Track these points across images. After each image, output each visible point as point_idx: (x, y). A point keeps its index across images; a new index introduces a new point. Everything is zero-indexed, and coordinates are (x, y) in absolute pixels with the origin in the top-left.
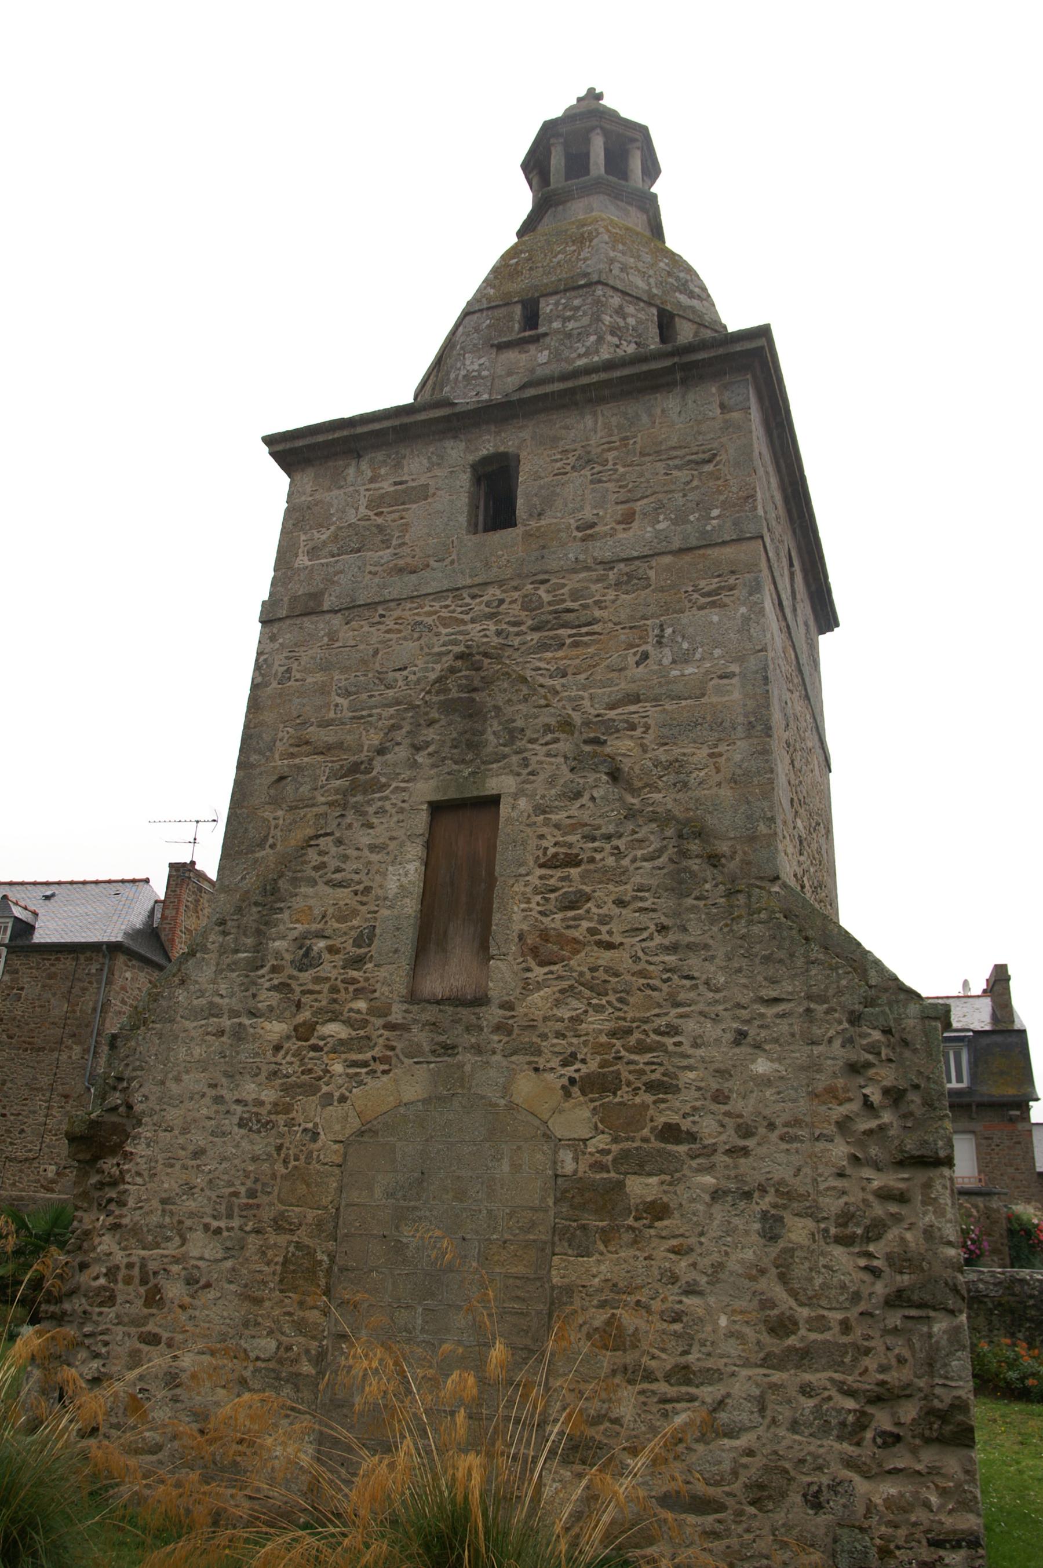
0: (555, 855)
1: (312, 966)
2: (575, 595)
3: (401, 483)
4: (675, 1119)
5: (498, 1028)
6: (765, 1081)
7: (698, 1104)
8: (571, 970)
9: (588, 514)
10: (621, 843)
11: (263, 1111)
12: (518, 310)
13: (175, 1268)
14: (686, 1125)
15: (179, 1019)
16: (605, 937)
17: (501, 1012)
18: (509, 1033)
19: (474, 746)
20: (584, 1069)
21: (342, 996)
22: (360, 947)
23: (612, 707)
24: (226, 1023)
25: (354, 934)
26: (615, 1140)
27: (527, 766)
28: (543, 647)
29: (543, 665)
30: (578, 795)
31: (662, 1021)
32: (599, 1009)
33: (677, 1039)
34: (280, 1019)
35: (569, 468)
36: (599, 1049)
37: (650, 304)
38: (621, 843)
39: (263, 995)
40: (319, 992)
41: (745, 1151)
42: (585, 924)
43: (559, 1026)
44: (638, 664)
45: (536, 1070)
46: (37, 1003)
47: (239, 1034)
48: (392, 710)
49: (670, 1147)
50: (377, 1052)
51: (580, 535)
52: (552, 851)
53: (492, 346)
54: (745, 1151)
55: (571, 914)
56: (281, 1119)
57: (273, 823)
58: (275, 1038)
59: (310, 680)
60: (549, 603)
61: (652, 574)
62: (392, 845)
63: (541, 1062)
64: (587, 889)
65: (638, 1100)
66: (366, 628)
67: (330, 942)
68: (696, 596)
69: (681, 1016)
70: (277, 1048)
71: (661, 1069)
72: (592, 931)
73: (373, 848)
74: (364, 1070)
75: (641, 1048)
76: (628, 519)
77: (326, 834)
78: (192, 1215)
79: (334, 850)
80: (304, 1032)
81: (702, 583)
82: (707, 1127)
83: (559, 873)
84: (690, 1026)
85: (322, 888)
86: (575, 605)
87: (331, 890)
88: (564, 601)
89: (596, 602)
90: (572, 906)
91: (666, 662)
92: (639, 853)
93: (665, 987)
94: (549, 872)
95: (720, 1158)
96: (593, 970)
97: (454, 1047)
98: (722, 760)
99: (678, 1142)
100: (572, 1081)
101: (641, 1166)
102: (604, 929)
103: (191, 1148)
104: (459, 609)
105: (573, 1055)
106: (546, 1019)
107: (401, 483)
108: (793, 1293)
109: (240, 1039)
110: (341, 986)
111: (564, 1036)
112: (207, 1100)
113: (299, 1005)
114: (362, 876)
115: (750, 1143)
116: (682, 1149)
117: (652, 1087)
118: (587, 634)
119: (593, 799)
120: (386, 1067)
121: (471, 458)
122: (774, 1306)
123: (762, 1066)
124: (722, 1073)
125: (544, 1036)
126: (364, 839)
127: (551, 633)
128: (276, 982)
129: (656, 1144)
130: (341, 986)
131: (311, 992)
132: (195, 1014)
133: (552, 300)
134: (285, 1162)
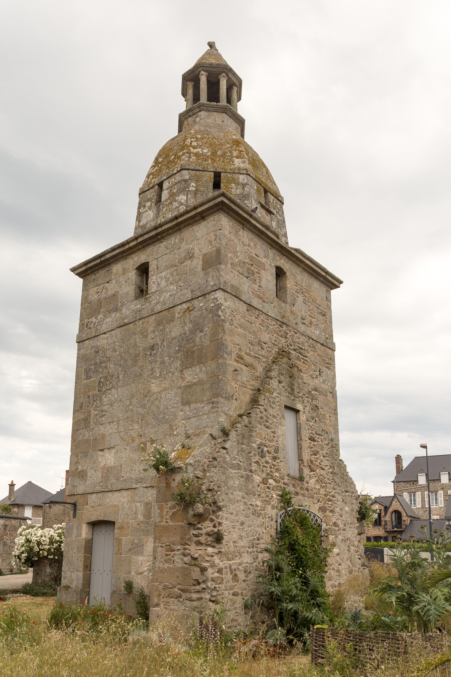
3: (257, 256)
104: (278, 329)
105: (319, 500)
130: (273, 466)
132: (233, 467)
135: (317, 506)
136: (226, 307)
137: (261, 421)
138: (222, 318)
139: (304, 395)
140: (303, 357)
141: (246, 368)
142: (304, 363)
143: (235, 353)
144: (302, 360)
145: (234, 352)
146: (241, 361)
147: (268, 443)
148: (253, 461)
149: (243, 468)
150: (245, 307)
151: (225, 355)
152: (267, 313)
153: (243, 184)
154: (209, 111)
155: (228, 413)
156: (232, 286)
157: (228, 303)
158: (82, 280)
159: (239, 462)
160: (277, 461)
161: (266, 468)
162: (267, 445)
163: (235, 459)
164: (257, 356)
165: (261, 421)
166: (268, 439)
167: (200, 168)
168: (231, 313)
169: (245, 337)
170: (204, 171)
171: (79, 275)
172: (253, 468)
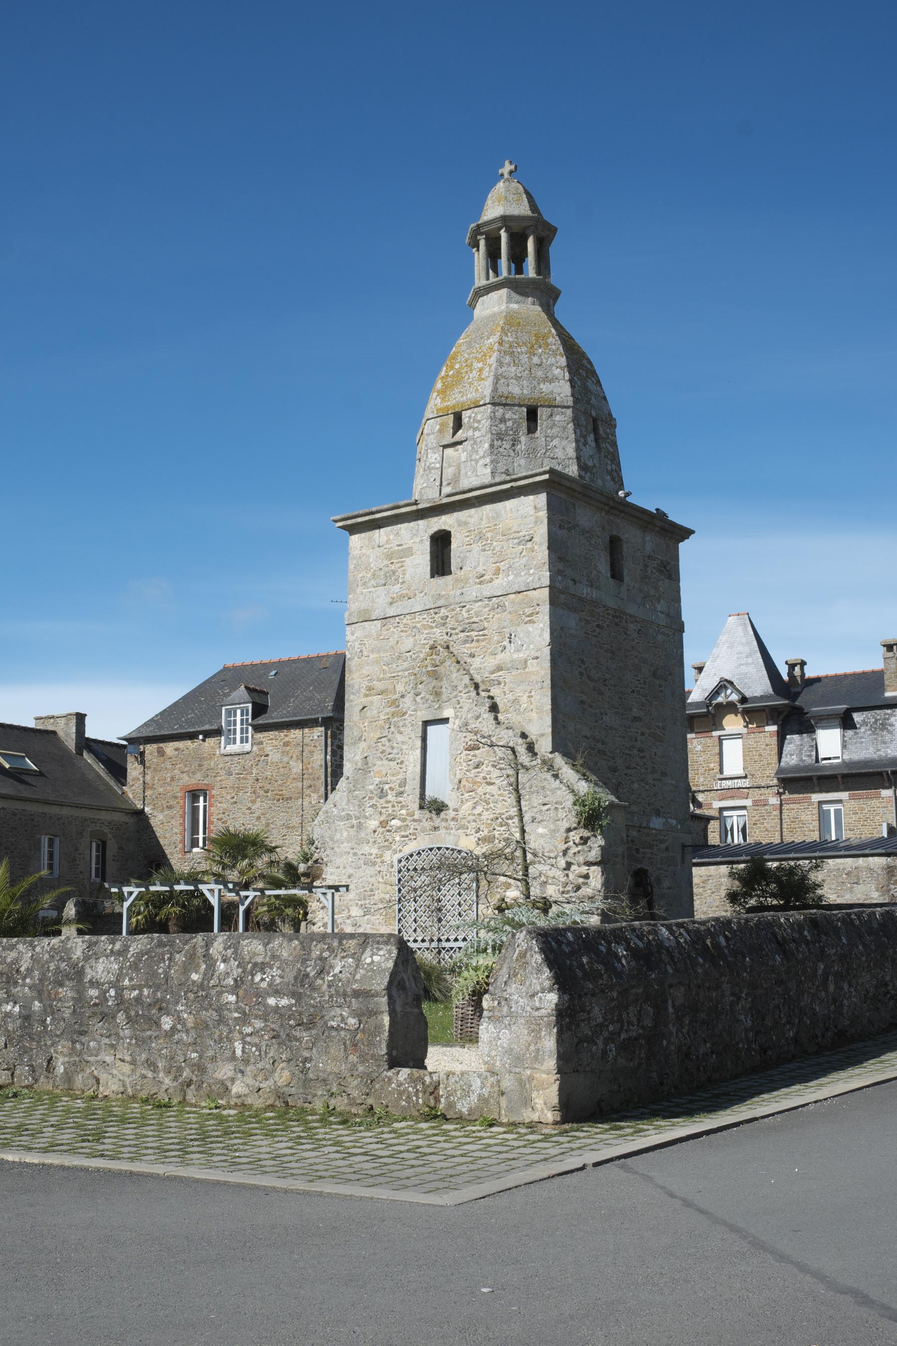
3: (400, 545)
5: (453, 819)
6: (542, 836)
9: (480, 569)
11: (372, 857)
12: (451, 417)
13: (348, 921)
19: (437, 694)
21: (396, 809)
23: (493, 673)
24: (354, 822)
28: (465, 642)
32: (487, 810)
37: (520, 406)
39: (367, 809)
42: (482, 775)
43: (473, 818)
44: (502, 651)
46: (280, 765)
48: (406, 673)
50: (411, 831)
52: (469, 743)
56: (379, 860)
58: (373, 827)
59: (371, 656)
60: (467, 618)
63: (468, 832)
66: (392, 629)
68: (524, 617)
70: (375, 832)
72: (485, 778)
73: (403, 743)
76: (497, 572)
78: (351, 900)
80: (384, 824)
83: (472, 753)
85: (385, 762)
86: (476, 620)
90: (477, 767)
96: (485, 794)
100: (479, 839)
107: (400, 545)
112: (351, 855)
113: (381, 813)
114: (399, 755)
121: (431, 531)
123: (541, 830)
125: (469, 822)
132: (341, 819)
134: (383, 878)
135: (473, 839)
139: (460, 692)
140: (477, 633)
142: (478, 641)
147: (390, 778)
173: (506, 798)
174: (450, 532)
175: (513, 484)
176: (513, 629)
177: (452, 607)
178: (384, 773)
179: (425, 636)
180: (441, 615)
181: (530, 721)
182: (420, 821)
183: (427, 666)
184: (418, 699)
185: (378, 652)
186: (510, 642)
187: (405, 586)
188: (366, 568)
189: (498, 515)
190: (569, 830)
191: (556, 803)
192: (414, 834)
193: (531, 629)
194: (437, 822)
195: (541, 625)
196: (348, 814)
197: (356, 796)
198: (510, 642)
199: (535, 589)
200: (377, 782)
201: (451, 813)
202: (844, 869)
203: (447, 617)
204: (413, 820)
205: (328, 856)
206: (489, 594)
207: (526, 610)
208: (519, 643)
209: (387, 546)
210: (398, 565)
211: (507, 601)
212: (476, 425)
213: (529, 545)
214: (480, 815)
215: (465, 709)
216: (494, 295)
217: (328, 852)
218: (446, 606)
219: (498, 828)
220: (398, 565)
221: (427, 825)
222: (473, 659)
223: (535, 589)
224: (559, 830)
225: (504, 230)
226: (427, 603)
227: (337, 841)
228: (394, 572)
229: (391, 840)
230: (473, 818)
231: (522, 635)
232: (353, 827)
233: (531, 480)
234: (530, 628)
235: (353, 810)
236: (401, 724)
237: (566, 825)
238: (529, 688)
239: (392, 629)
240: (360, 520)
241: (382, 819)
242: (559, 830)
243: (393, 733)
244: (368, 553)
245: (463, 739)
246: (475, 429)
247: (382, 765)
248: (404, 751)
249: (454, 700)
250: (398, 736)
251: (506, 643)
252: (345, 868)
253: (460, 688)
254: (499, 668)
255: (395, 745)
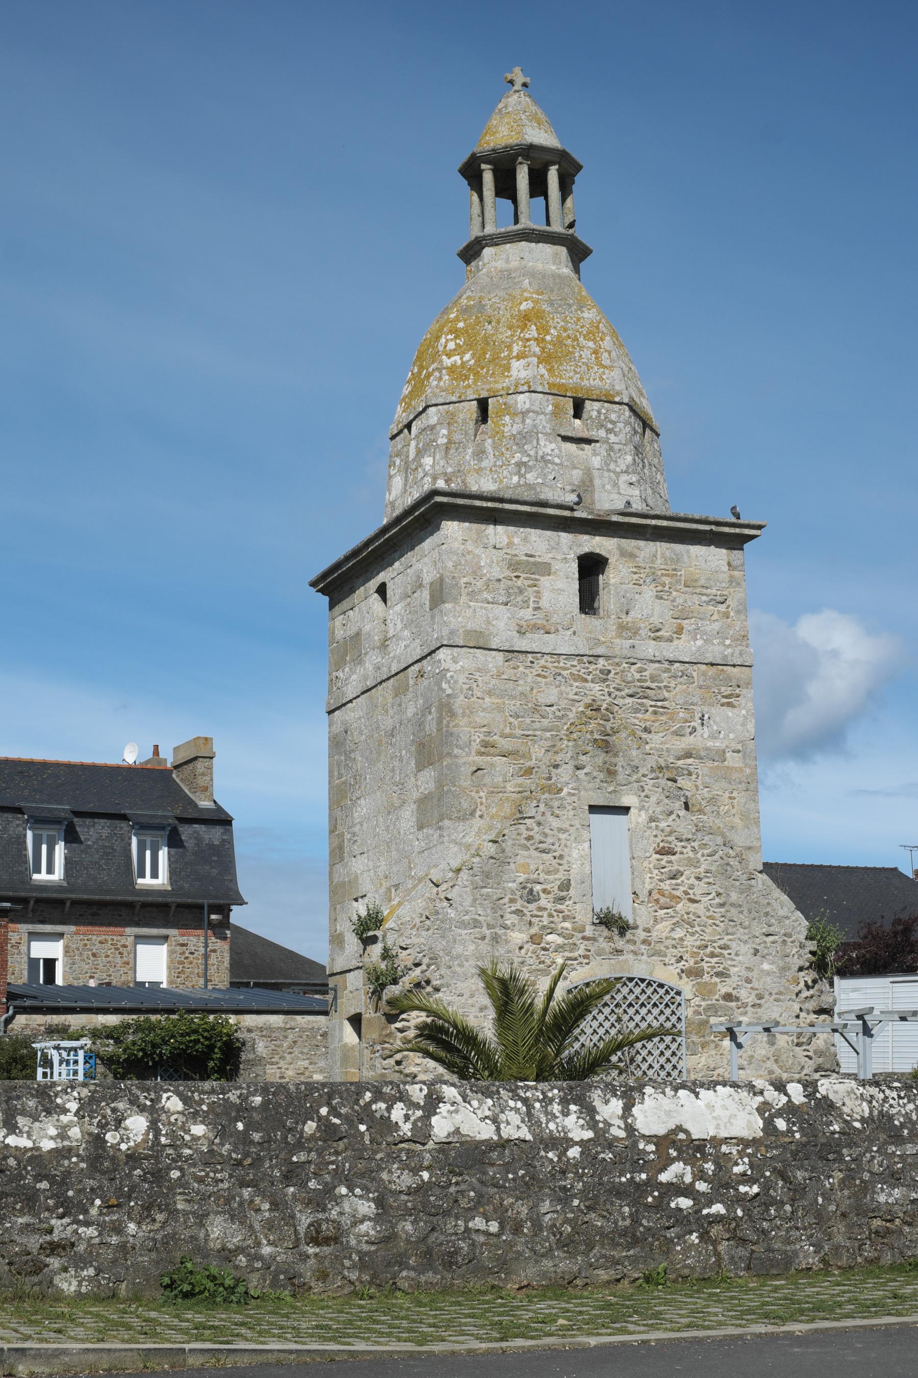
0: (663, 848)
1: (536, 901)
2: (653, 679)
3: (531, 556)
4: (730, 990)
5: (644, 942)
6: (768, 973)
7: (739, 983)
8: (677, 913)
10: (695, 844)
14: (734, 993)
15: (453, 928)
16: (692, 896)
17: (644, 933)
18: (650, 945)
19: (611, 773)
20: (687, 965)
22: (562, 891)
23: (679, 759)
25: (558, 883)
26: (704, 1000)
27: (643, 791)
28: (637, 711)
29: (637, 722)
30: (671, 813)
31: (721, 942)
32: (692, 934)
33: (729, 951)
34: (520, 931)
35: (642, 581)
36: (694, 955)
38: (695, 844)
39: (507, 916)
40: (542, 917)
41: (760, 1005)
42: (682, 889)
43: (674, 942)
44: (691, 734)
45: (665, 964)
47: (496, 939)
48: (548, 734)
49: (728, 1004)
51: (652, 635)
52: (661, 845)
53: (559, 435)
54: (760, 1005)
55: (674, 882)
57: (479, 800)
58: (519, 942)
59: (487, 699)
60: (639, 680)
61: (695, 674)
62: (572, 830)
63: (667, 960)
64: (681, 869)
65: (713, 981)
67: (543, 886)
69: (730, 940)
70: (521, 948)
71: (722, 966)
73: (560, 830)
74: (575, 962)
75: (712, 955)
77: (530, 818)
79: (536, 828)
80: (535, 939)
81: (723, 689)
82: (743, 994)
83: (665, 858)
84: (733, 945)
86: (653, 685)
87: (539, 854)
88: (646, 681)
89: (665, 687)
91: (706, 736)
92: (706, 852)
93: (722, 925)
94: (661, 857)
95: (749, 1009)
96: (688, 913)
97: (622, 951)
98: (735, 801)
99: (732, 1001)
100: (682, 971)
101: (716, 1012)
102: (691, 892)
103: (478, 1005)
104: (583, 671)
105: (681, 957)
106: (667, 938)
107: (531, 556)
108: (781, 1068)
109: (497, 942)
110: (555, 914)
111: (676, 948)
113: (530, 923)
115: (762, 1002)
116: (733, 1004)
117: (718, 974)
118: (662, 707)
119: (678, 816)
120: (587, 961)
122: (774, 1073)
123: (766, 966)
124: (749, 969)
125: (667, 948)
126: (555, 823)
127: (639, 701)
128: (513, 909)
129: (722, 1002)
130: (555, 914)
131: (537, 916)
132: (463, 925)
133: (597, 405)
135: (674, 970)
136: (455, 672)
137: (528, 844)
138: (449, 691)
139: (644, 776)
140: (653, 703)
141: (505, 759)
142: (655, 713)
143: (478, 740)
144: (651, 709)
145: (475, 741)
146: (492, 750)
147: (542, 877)
148: (509, 910)
149: (485, 925)
150: (500, 656)
151: (456, 751)
152: (554, 652)
153: (522, 413)
154: (497, 245)
155: (464, 841)
156: (468, 633)
157: (461, 663)
158: (327, 598)
159: (477, 917)
160: (567, 903)
161: (538, 919)
162: (542, 880)
163: (467, 912)
164: (530, 733)
165: (528, 844)
166: (543, 871)
167: (454, 399)
168: (467, 678)
169: (500, 709)
170: (460, 402)
171: (322, 591)
172: (508, 922)
173: (717, 922)
174: (607, 559)
175: (713, 527)
176: (706, 709)
177: (617, 660)
178: (532, 867)
179: (575, 690)
180: (599, 666)
181: (733, 827)
182: (594, 939)
183: (592, 732)
184: (581, 773)
185: (501, 696)
186: (703, 724)
187: (540, 614)
188: (474, 572)
189: (678, 559)
190: (801, 969)
191: (785, 935)
192: (585, 957)
193: (730, 714)
194: (620, 943)
195: (744, 712)
196: (475, 920)
197: (488, 895)
198: (703, 724)
199: (734, 666)
200: (521, 880)
201: (641, 934)
202: (319, 1029)
203: (609, 671)
204: (583, 938)
205: (442, 977)
206: (671, 657)
207: (723, 689)
208: (715, 728)
209: (509, 551)
210: (527, 583)
211: (694, 671)
212: (610, 426)
213: (722, 608)
214: (681, 939)
215: (653, 799)
216: (547, 249)
217: (443, 971)
218: (607, 658)
219: (706, 959)
220: (527, 583)
221: (603, 944)
222: (650, 736)
223: (734, 666)
224: (789, 969)
225: (557, 167)
226: (581, 646)
227: (458, 957)
228: (521, 591)
229: (548, 962)
230: (674, 942)
231: (718, 719)
232: (483, 938)
233: (738, 531)
234: (729, 712)
235: (484, 915)
236: (556, 804)
237: (801, 963)
238: (731, 787)
239: (521, 669)
240: (478, 503)
241: (533, 931)
242: (789, 969)
243: (543, 814)
244: (477, 551)
245: (652, 838)
246: (609, 431)
247: (530, 857)
248: (563, 842)
249: (635, 785)
250: (551, 819)
251: (697, 723)
252: (472, 996)
253: (643, 771)
254: (688, 755)
255: (547, 831)
